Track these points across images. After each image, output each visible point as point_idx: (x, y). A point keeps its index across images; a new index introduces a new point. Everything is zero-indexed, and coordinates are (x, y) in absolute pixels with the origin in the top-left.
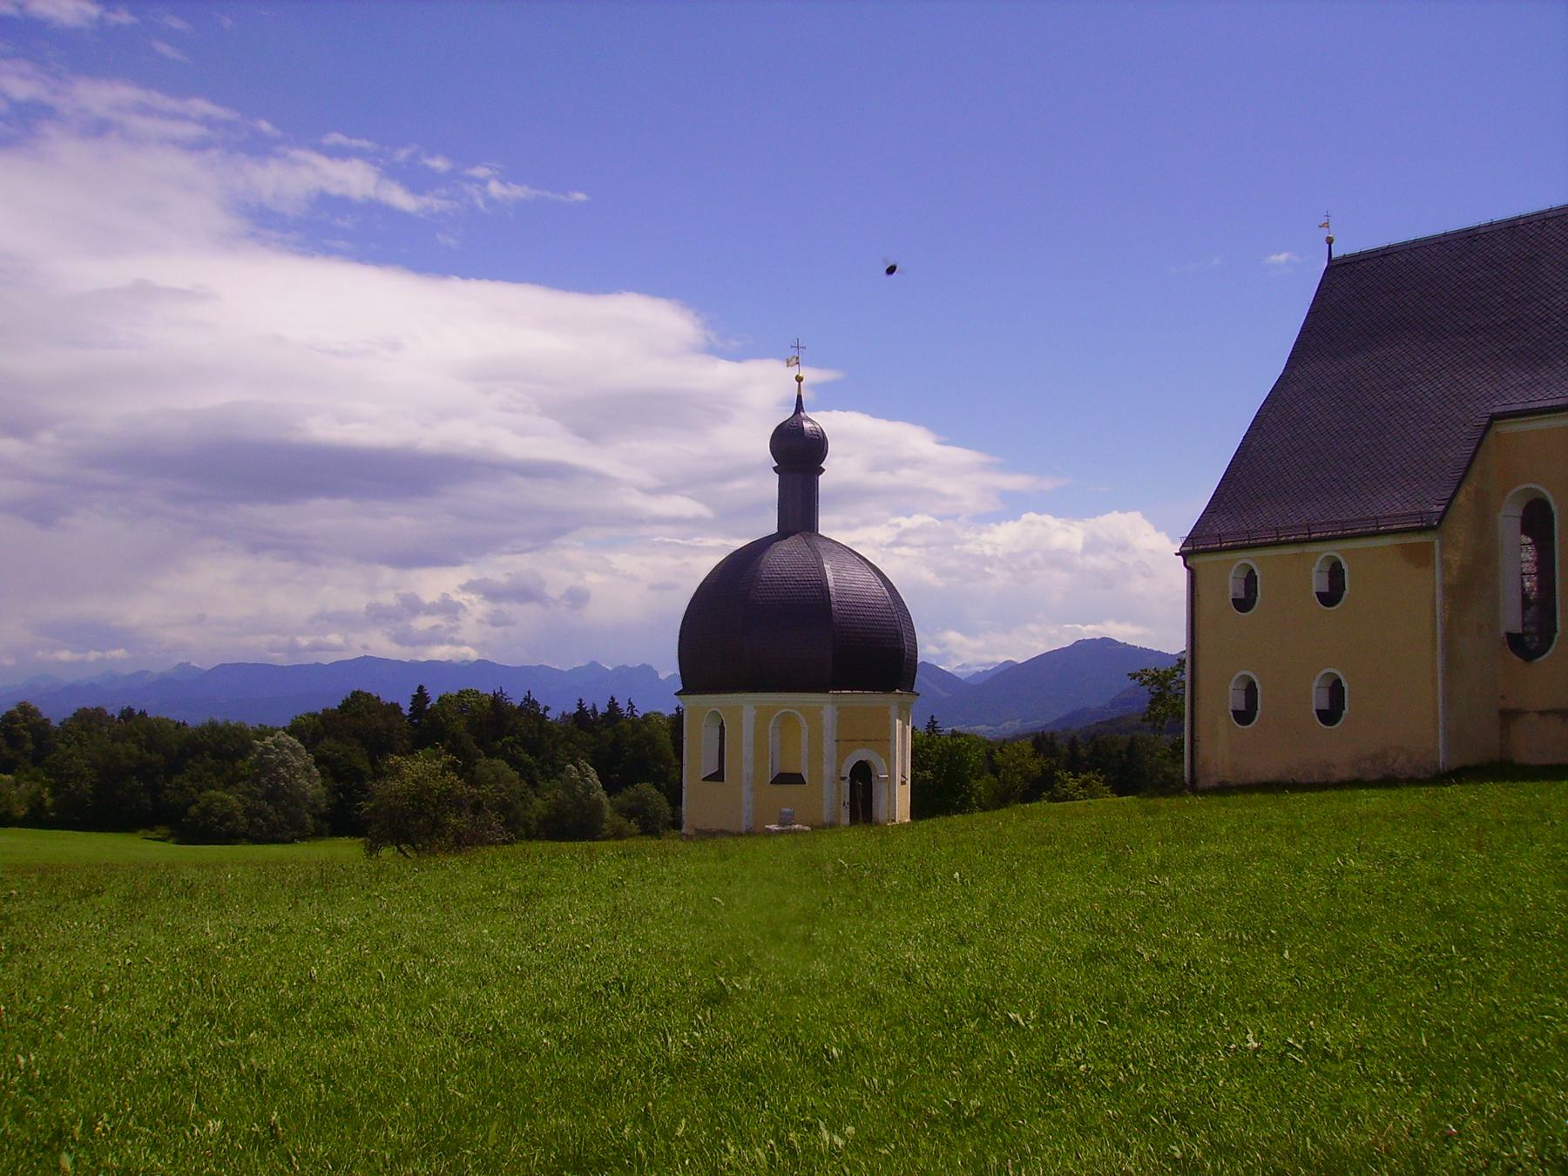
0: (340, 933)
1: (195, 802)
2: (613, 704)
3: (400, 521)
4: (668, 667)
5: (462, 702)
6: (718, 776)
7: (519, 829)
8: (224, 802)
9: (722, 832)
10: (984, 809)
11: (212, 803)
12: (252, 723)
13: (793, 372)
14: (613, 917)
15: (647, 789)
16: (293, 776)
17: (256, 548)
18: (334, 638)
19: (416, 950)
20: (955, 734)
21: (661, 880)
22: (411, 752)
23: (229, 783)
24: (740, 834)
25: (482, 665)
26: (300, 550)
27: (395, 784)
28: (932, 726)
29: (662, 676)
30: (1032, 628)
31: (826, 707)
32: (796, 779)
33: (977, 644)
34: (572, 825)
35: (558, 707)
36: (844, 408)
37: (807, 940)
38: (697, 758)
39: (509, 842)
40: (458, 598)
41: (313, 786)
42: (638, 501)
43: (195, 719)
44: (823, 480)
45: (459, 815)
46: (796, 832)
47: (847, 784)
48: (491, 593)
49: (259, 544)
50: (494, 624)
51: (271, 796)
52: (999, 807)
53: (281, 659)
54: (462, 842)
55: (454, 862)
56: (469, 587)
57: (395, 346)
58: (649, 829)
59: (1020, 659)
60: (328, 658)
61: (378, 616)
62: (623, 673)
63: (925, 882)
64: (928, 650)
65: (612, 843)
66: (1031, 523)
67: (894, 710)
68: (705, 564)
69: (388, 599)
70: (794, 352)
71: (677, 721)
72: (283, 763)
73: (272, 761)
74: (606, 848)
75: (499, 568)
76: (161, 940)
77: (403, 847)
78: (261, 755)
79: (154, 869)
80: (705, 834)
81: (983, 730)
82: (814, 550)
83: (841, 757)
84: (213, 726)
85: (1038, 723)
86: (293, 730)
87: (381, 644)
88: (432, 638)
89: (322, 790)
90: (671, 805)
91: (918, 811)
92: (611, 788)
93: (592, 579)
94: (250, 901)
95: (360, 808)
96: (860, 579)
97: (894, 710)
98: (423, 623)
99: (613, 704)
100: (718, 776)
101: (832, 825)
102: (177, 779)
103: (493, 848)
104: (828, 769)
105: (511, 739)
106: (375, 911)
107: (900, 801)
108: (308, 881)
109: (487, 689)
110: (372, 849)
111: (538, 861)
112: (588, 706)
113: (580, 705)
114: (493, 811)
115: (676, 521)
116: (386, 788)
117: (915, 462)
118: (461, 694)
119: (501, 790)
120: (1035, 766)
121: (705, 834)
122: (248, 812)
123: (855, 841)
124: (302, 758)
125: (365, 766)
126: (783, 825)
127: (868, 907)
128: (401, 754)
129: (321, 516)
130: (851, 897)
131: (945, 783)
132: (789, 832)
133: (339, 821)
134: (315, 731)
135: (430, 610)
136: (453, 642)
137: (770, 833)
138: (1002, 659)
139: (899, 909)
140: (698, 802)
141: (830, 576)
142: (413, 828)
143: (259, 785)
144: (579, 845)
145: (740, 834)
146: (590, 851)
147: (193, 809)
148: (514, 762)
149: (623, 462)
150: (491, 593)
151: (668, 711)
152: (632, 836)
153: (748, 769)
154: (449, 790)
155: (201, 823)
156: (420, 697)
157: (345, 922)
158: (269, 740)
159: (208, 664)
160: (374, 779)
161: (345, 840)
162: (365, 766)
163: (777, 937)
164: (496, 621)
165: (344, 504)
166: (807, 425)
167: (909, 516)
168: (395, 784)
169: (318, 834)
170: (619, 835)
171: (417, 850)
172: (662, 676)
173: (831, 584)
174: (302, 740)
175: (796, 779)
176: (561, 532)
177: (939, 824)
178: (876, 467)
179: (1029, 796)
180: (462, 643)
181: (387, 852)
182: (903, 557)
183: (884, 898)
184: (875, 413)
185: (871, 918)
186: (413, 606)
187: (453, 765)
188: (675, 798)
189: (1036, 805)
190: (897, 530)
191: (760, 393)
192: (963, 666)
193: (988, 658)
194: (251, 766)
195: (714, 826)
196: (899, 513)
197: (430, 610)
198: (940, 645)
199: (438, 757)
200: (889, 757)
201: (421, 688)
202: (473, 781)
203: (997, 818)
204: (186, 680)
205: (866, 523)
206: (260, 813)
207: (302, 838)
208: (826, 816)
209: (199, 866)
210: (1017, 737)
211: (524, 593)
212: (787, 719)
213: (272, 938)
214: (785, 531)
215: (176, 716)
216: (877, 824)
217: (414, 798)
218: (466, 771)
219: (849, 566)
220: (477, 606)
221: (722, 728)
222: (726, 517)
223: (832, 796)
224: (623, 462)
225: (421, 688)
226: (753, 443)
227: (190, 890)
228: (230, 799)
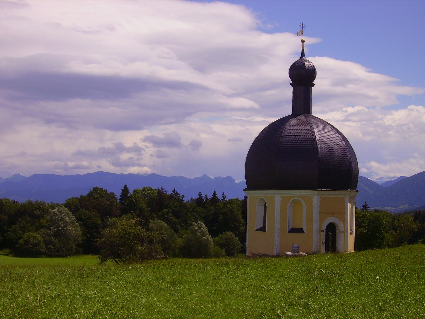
0: (89, 298)
1: (22, 238)
2: (215, 195)
3: (113, 109)
4: (240, 177)
5: (145, 193)
6: (263, 229)
7: (170, 251)
8: (35, 238)
9: (265, 255)
10: (389, 246)
11: (29, 238)
12: (48, 201)
13: (300, 38)
14: (215, 293)
15: (229, 234)
16: (65, 226)
17: (49, 122)
18: (85, 163)
19: (123, 307)
20: (376, 211)
21: (237, 277)
22: (121, 216)
23: (37, 229)
24: (273, 256)
25: (153, 176)
26: (69, 123)
27: (113, 231)
28: (365, 207)
29: (237, 182)
30: (412, 160)
31: (315, 197)
32: (300, 231)
33: (386, 168)
34: (194, 251)
35: (189, 196)
36: (321, 56)
37: (306, 306)
38: (254, 220)
39: (165, 258)
40: (141, 145)
41: (75, 230)
42: (224, 100)
43: (22, 200)
44: (313, 89)
45: (142, 245)
46: (301, 256)
47: (324, 234)
48: (157, 142)
49: (50, 120)
50: (159, 157)
51: (57, 235)
52: (397, 246)
53: (61, 172)
54: (144, 258)
55: (140, 267)
56: (146, 139)
57: (112, 29)
58: (230, 253)
59: (408, 175)
60: (82, 172)
61: (105, 153)
62: (219, 180)
63: (364, 280)
64: (363, 171)
65: (214, 259)
66: (411, 110)
67: (347, 199)
68: (257, 129)
69: (109, 145)
70: (300, 29)
71: (245, 202)
72: (62, 220)
73: (56, 219)
74: (211, 261)
75: (160, 132)
76: (7, 300)
77: (117, 260)
78: (52, 216)
79: (3, 268)
80: (256, 256)
81: (389, 209)
82: (310, 123)
83: (322, 221)
84: (30, 203)
85: (416, 206)
86: (67, 205)
87: (107, 166)
88: (130, 163)
89: (80, 233)
90: (240, 242)
91: (358, 246)
92: (213, 233)
93: (204, 136)
94: (47, 283)
95: (97, 241)
96: (333, 136)
97: (347, 199)
98: (125, 157)
99: (215, 195)
100: (263, 229)
101: (316, 253)
102: (13, 227)
103: (158, 261)
104: (315, 226)
105: (167, 210)
106: (104, 288)
107: (350, 242)
108: (73, 274)
109: (156, 187)
110: (102, 261)
111: (179, 267)
112: (203, 196)
113: (200, 195)
114: (158, 243)
115: (242, 109)
116: (110, 232)
117: (356, 81)
118: (144, 190)
119: (162, 234)
120: (415, 226)
121: (256, 256)
122: (45, 242)
123: (328, 259)
124: (69, 218)
125: (100, 222)
126: (293, 252)
127: (335, 291)
128: (117, 217)
129: (77, 107)
130: (326, 287)
131: (371, 235)
132: (297, 256)
133: (87, 247)
134: (76, 206)
135: (129, 150)
136: (139, 165)
137: (287, 256)
138: (398, 175)
139: (349, 293)
140: (254, 241)
141: (317, 135)
142: (121, 251)
143: (50, 230)
144: (200, 260)
145: (273, 256)
146: (204, 263)
147: (21, 241)
148: (168, 221)
149: (217, 80)
150: (157, 142)
151: (242, 198)
152: (222, 256)
153: (277, 226)
154: (138, 234)
155: (24, 248)
156: (125, 190)
157: (91, 293)
158: (55, 210)
159: (27, 174)
160: (103, 228)
161: (90, 256)
162: (100, 222)
163: (291, 304)
164: (160, 155)
165: (88, 101)
166: (306, 63)
167: (353, 107)
168: (113, 231)
169: (77, 253)
170: (216, 256)
171: (123, 262)
172: (237, 182)
173: (317, 139)
174: (70, 210)
175: (300, 231)
176: (189, 114)
177: (369, 253)
178: (337, 83)
179: (411, 242)
180: (144, 165)
181: (109, 262)
182: (349, 126)
183: (342, 288)
184: (336, 58)
185: (336, 297)
186: (120, 148)
187: (140, 223)
188: (243, 238)
189: (416, 246)
190: (346, 114)
191: (283, 49)
192: (380, 178)
193: (392, 175)
194: (47, 222)
195: (261, 252)
196: (348, 105)
197: (129, 150)
198: (368, 168)
199: (133, 218)
200: (344, 221)
201: (125, 187)
202: (149, 230)
203: (396, 251)
204: (18, 182)
205: (333, 110)
206: (52, 243)
207: (70, 255)
208: (314, 249)
209: (24, 267)
210: (407, 213)
211: (172, 142)
212: (296, 203)
213: (57, 301)
214: (295, 114)
215: (13, 198)
216: (338, 253)
217: (122, 237)
218: (145, 224)
219: (326, 130)
220: (150, 150)
221: (265, 206)
222: (265, 108)
223: (316, 238)
224: (217, 80)
225: (125, 187)
226: (280, 72)
227: (20, 278)
228: (37, 236)
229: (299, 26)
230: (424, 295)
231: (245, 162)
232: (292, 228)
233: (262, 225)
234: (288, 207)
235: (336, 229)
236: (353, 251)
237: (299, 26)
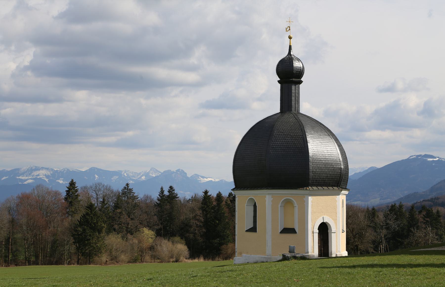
6: (253, 229)
32: (291, 231)
100: (253, 229)
175: (291, 231)
200: (335, 220)
221: (255, 206)
229: (287, 21)
230: (373, 285)
231: (232, 161)
232: (284, 228)
233: (252, 226)
234: (279, 207)
235: (328, 229)
236: (345, 254)
237: (287, 21)
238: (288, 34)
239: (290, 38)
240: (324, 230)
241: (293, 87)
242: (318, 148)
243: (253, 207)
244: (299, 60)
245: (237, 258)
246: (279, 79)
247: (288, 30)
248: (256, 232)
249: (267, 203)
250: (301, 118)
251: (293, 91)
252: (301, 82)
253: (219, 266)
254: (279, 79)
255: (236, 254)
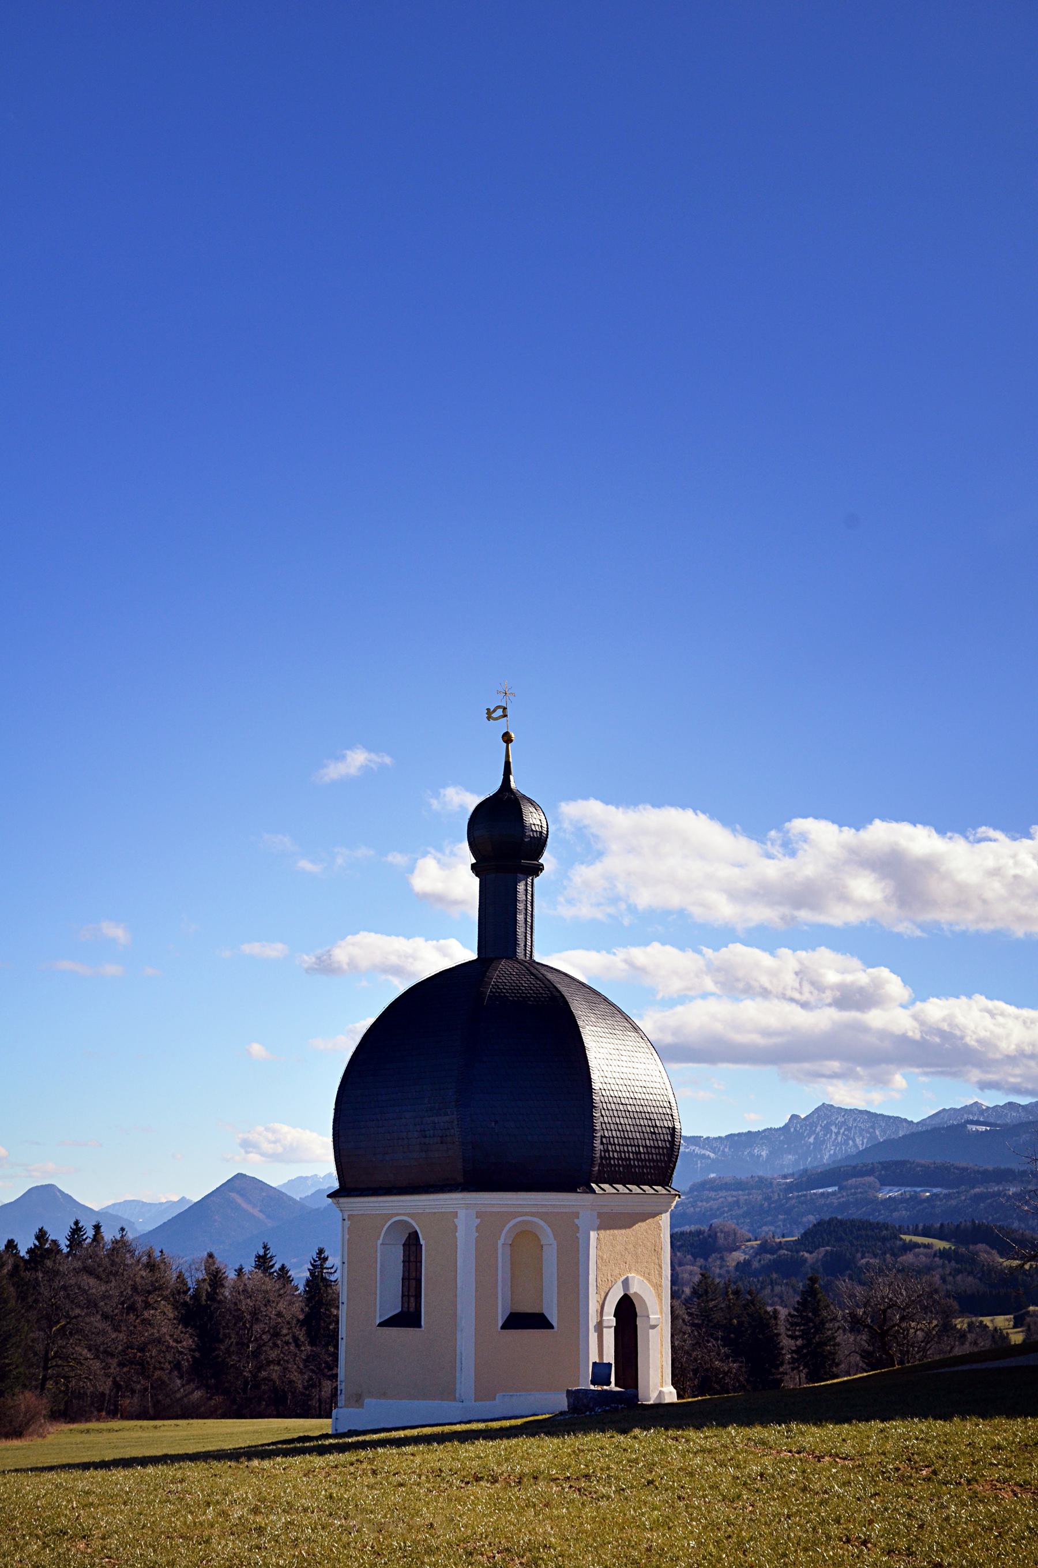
6: (408, 1317)
32: (538, 1321)
100: (408, 1317)
175: (538, 1321)
229: (498, 692)
233: (395, 1308)
238: (500, 727)
239: (507, 738)
240: (627, 1312)
241: (521, 887)
242: (619, 1068)
243: (400, 1250)
244: (532, 802)
245: (344, 1410)
246: (474, 861)
247: (500, 712)
248: (420, 1326)
249: (460, 1234)
250: (550, 976)
251: (521, 896)
252: (538, 870)
253: (85, 1466)
254: (474, 861)
255: (341, 1399)
